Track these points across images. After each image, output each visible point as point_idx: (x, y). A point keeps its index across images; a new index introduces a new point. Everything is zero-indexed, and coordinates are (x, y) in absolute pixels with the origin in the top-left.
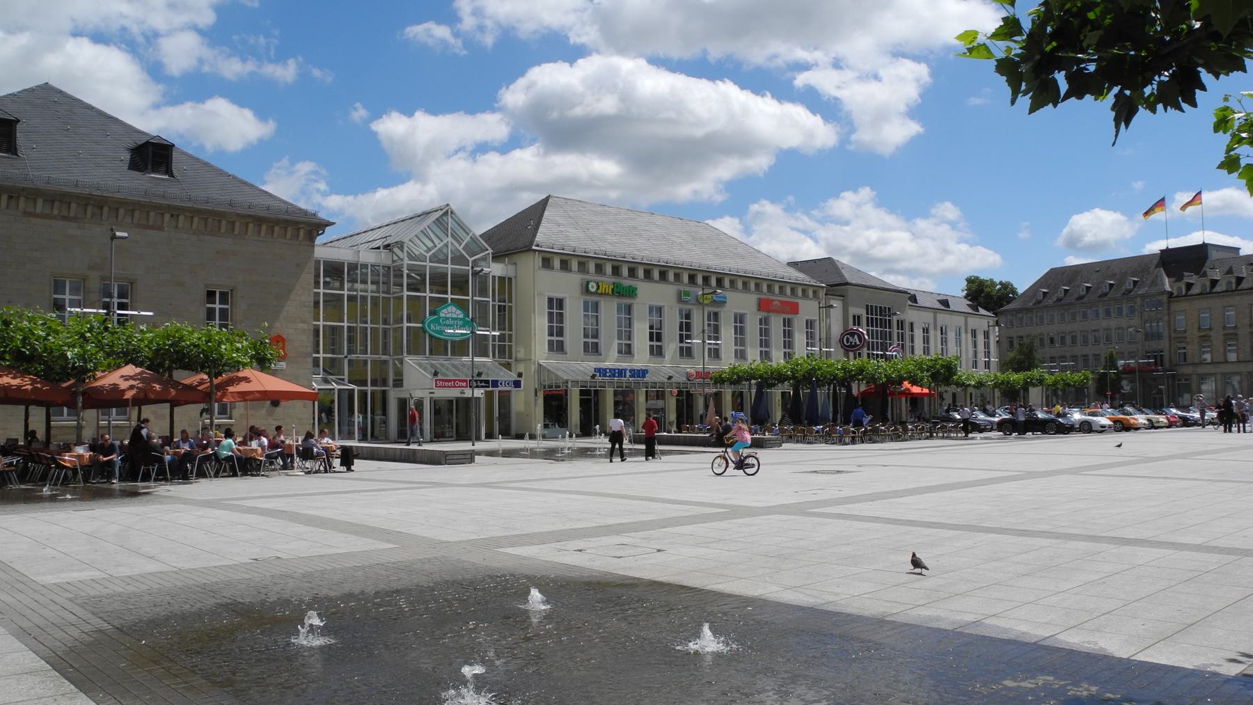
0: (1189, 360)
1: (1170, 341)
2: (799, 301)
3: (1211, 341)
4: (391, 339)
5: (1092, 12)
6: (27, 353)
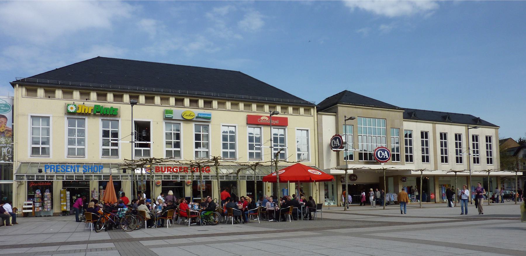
2: (289, 117)
4: (385, 187)
6: (3, 199)
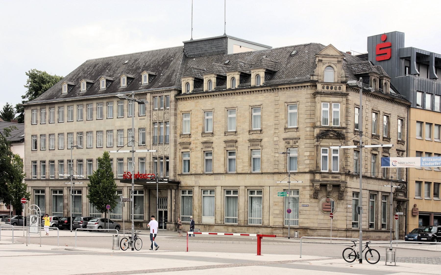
0: (193, 171)
1: (175, 145)
3: (237, 147)
5: (362, 218)
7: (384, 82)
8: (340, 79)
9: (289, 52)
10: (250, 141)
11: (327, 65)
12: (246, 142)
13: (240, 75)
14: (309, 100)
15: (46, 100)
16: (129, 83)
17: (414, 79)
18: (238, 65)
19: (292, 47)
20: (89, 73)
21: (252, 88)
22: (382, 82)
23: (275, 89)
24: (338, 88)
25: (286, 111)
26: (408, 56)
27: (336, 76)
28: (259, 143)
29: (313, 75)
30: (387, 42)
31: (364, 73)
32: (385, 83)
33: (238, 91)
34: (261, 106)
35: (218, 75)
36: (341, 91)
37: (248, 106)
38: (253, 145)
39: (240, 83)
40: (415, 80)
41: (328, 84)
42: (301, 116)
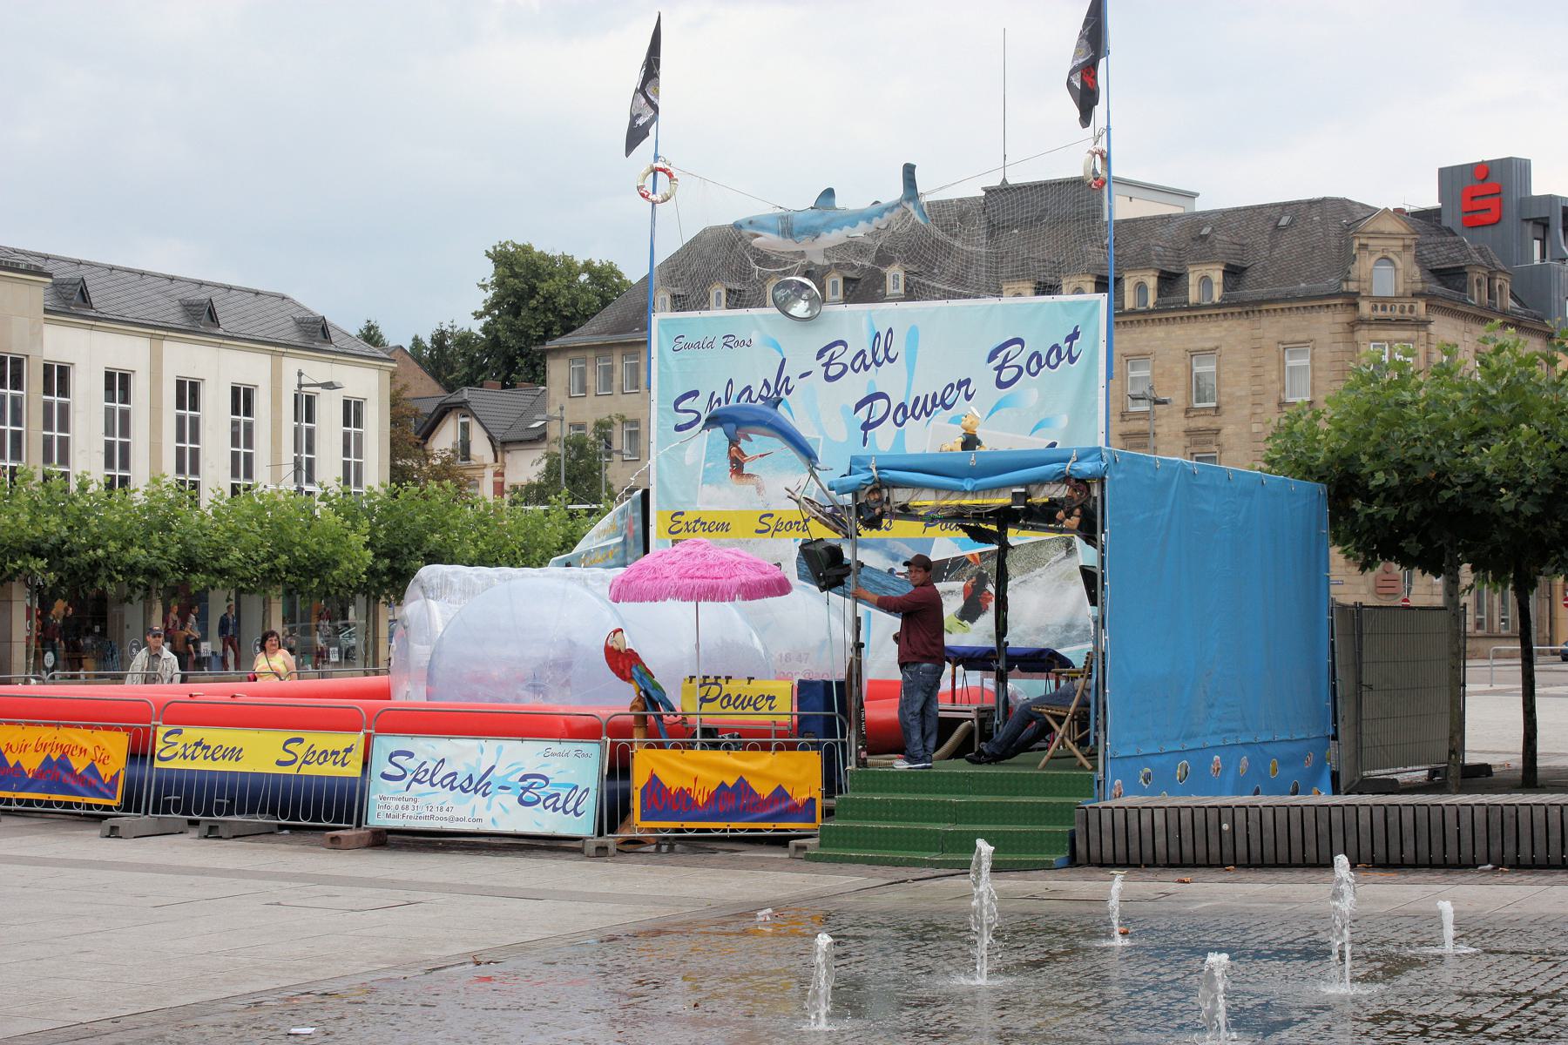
7: (1498, 283)
8: (1408, 286)
9: (1269, 218)
10: (1189, 432)
11: (1379, 255)
12: (1177, 436)
13: (1159, 277)
14: (1339, 338)
15: (611, 334)
16: (848, 293)
17: (1559, 271)
18: (1153, 253)
19: (1276, 205)
20: (719, 262)
21: (1190, 309)
22: (1494, 284)
23: (1253, 311)
24: (1407, 309)
25: (1281, 361)
26: (1544, 215)
27: (1400, 280)
28: (1213, 438)
29: (1347, 280)
30: (1489, 181)
31: (1454, 265)
32: (1500, 286)
33: (1155, 316)
34: (1217, 351)
35: (1099, 277)
36: (1414, 315)
37: (1182, 351)
38: (1196, 444)
39: (1159, 296)
40: (1562, 274)
41: (1384, 300)
42: (1319, 374)
